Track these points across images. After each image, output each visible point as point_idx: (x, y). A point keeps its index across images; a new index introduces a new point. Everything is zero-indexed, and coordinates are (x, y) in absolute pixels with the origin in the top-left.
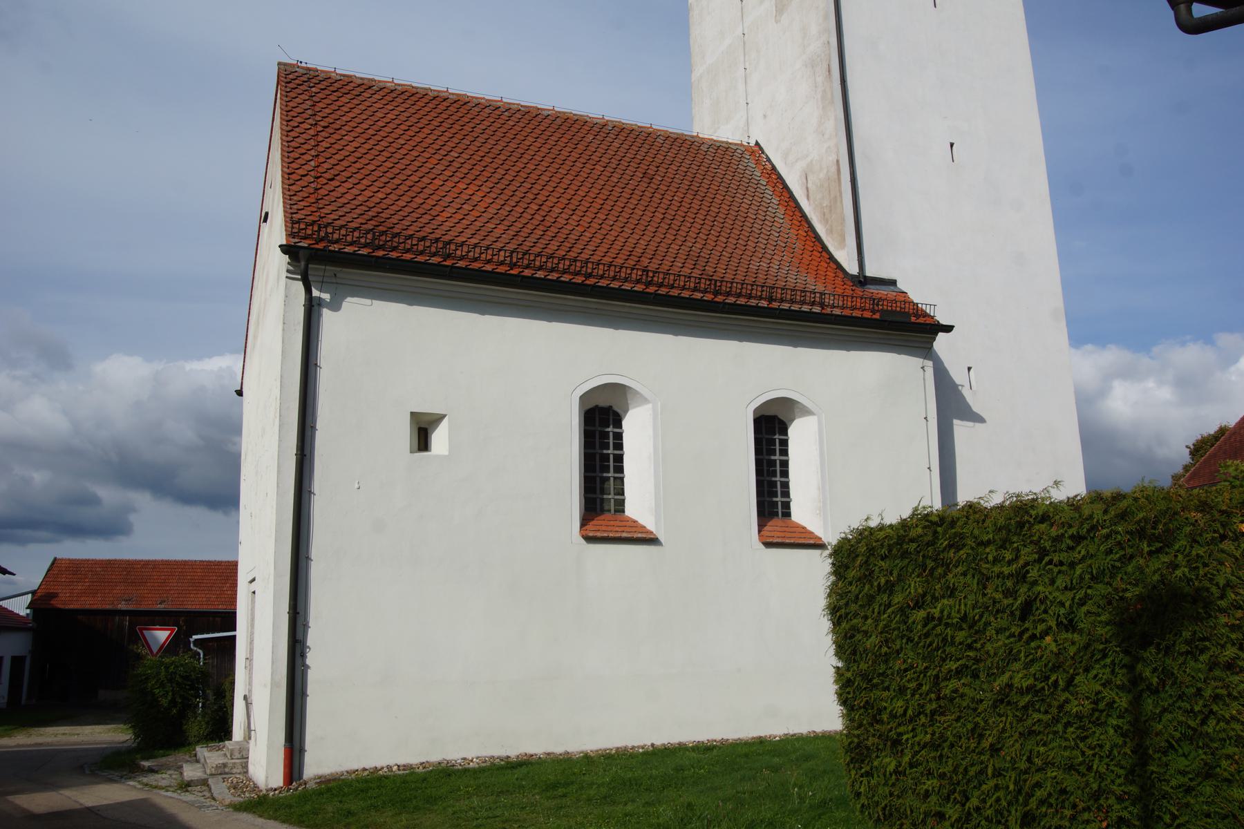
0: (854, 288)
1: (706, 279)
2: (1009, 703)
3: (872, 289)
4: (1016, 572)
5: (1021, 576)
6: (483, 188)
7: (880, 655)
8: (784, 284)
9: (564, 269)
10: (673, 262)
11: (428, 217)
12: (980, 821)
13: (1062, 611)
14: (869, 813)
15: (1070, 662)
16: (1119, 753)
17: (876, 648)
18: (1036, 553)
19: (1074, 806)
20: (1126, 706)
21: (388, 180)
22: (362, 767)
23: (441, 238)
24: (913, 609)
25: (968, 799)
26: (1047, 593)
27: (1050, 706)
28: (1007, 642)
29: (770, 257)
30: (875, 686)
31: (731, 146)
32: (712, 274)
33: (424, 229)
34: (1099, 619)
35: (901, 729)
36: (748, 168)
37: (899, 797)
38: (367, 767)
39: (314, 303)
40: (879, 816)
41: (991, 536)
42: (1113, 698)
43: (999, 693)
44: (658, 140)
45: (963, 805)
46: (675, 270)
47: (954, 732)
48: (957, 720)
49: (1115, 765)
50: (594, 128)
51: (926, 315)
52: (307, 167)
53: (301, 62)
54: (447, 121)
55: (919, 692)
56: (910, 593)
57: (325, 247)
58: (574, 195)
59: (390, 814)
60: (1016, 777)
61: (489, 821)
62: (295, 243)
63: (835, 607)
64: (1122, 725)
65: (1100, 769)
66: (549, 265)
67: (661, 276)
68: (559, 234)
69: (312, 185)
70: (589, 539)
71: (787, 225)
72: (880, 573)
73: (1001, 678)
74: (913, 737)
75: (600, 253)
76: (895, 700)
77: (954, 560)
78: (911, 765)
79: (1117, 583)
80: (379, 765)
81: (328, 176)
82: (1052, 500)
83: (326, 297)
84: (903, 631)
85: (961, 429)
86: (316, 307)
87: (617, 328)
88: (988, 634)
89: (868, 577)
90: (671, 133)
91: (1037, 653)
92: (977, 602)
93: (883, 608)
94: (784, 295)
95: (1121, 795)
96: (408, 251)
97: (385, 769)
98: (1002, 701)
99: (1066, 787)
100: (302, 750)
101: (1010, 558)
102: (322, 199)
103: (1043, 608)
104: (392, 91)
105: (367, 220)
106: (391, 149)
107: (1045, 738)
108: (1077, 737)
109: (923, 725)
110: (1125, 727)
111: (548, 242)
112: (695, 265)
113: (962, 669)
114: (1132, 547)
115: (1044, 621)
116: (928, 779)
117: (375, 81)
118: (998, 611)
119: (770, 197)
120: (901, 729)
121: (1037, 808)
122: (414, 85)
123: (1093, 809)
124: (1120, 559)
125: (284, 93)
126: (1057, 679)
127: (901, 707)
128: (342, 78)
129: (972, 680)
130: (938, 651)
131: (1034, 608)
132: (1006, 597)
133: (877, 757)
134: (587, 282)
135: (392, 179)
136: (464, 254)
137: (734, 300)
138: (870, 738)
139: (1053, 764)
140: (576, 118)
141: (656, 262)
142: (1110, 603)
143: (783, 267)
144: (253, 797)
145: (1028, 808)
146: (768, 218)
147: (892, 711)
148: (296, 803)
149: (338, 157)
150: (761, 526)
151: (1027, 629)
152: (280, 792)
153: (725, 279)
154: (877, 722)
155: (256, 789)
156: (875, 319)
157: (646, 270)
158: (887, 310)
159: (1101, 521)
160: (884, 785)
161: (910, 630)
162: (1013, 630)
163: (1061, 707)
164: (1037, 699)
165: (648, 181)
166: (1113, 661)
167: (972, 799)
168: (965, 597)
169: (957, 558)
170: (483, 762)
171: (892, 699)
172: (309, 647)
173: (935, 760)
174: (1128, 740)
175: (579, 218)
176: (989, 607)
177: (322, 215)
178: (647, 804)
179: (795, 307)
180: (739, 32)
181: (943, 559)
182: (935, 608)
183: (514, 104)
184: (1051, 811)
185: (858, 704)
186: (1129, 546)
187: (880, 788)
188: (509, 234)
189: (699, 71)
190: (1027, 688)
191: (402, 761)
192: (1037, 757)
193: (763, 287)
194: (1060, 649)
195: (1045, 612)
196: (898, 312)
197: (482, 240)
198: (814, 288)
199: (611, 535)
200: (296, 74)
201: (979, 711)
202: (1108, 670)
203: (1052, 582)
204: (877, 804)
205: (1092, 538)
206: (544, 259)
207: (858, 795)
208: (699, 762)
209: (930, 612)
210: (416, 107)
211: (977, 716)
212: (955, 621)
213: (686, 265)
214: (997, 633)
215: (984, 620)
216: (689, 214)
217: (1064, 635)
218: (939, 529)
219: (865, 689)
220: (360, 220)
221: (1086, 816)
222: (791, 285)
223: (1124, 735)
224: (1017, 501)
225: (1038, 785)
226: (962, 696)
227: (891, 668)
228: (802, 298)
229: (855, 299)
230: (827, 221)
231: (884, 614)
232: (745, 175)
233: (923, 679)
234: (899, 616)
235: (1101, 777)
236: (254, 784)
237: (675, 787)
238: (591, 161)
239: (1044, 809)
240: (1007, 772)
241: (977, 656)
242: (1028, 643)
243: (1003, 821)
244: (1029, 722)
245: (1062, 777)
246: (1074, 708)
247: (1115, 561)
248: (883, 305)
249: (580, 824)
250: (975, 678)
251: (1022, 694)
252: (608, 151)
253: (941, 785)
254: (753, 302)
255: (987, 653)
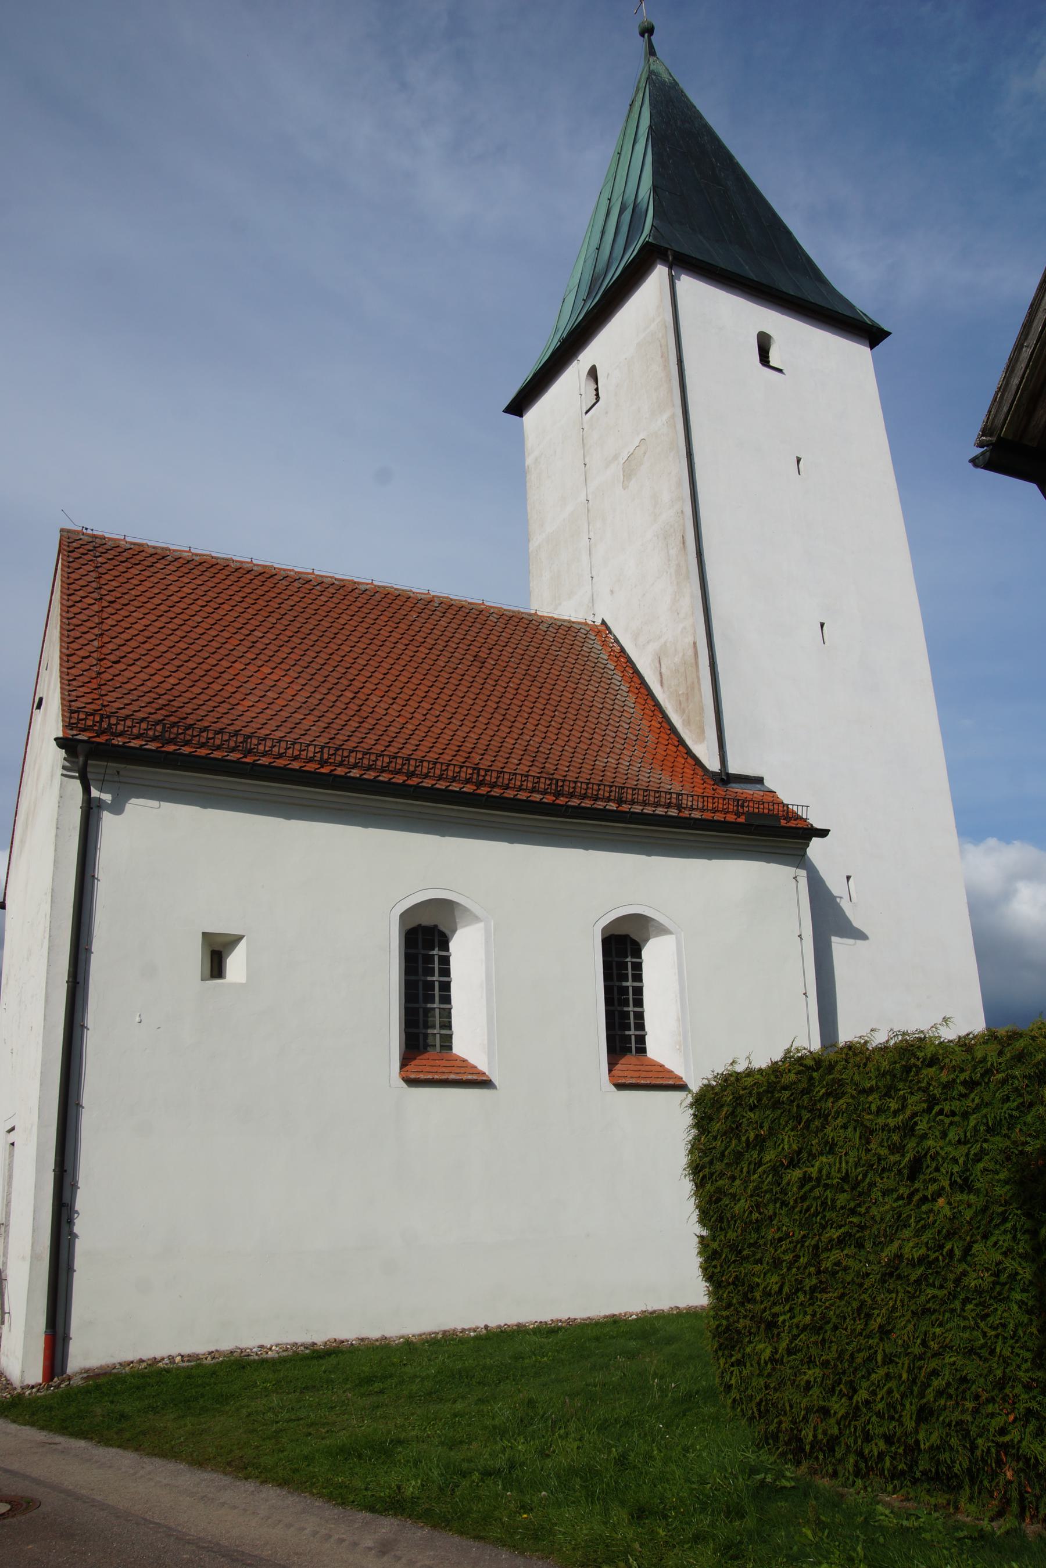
0: (715, 787)
1: (546, 778)
2: (899, 1277)
3: (736, 788)
4: (903, 1124)
5: (908, 1129)
6: (291, 673)
7: (751, 1221)
8: (636, 783)
9: (382, 767)
10: (508, 758)
11: (226, 706)
12: (870, 1418)
13: (956, 1169)
14: (742, 1410)
15: (966, 1228)
16: (1025, 1333)
17: (746, 1215)
18: (924, 1101)
19: (977, 1397)
20: (1030, 1278)
21: (181, 663)
22: (138, 1358)
23: (241, 730)
24: (787, 1167)
25: (855, 1391)
26: (938, 1148)
27: (945, 1279)
28: (895, 1205)
29: (619, 752)
30: (746, 1258)
31: (574, 625)
32: (553, 772)
33: (222, 720)
34: (997, 1177)
35: (776, 1309)
36: (593, 650)
37: (776, 1390)
38: (144, 1358)
39: (93, 805)
40: (753, 1413)
41: (874, 1082)
42: (1016, 1269)
43: (888, 1265)
44: (491, 618)
45: (851, 1398)
46: (510, 768)
47: (838, 1312)
48: (841, 1297)
49: (1021, 1348)
50: (418, 605)
51: (798, 818)
52: (89, 648)
53: (86, 529)
54: (251, 596)
55: (796, 1265)
56: (783, 1149)
57: (107, 740)
58: (394, 681)
59: (172, 1416)
60: (909, 1364)
61: (292, 1425)
62: (73, 735)
63: (697, 1166)
64: (1026, 1300)
65: (1004, 1352)
66: (366, 761)
67: (495, 774)
68: (377, 726)
69: (95, 669)
70: (411, 1082)
71: (638, 714)
72: (748, 1126)
73: (889, 1248)
74: (791, 1318)
75: (424, 748)
76: (769, 1275)
77: (833, 1111)
78: (790, 1352)
79: (1016, 1135)
80: (158, 1354)
81: (112, 658)
82: (942, 1040)
83: (107, 797)
84: (777, 1193)
85: (840, 947)
86: (95, 810)
87: (443, 835)
88: (873, 1196)
89: (734, 1131)
90: (505, 610)
91: (928, 1218)
92: (860, 1159)
93: (752, 1166)
94: (636, 796)
95: (1028, 1382)
96: (203, 745)
97: (166, 1361)
98: (891, 1274)
99: (967, 1374)
100: (66, 1338)
101: (896, 1107)
102: (105, 684)
103: (934, 1165)
104: (189, 562)
105: (157, 710)
106: (186, 628)
107: (941, 1317)
108: (978, 1315)
109: (801, 1304)
110: (1030, 1303)
111: (364, 736)
112: (533, 761)
113: (845, 1237)
114: (1030, 1094)
115: (935, 1180)
116: (809, 1368)
117: (170, 550)
118: (884, 1170)
119: (619, 684)
120: (776, 1309)
121: (935, 1400)
122: (214, 554)
123: (998, 1400)
124: (1017, 1108)
125: (67, 564)
126: (952, 1248)
127: (776, 1283)
128: (132, 546)
129: (856, 1250)
130: (816, 1217)
131: (924, 1166)
132: (893, 1154)
133: (750, 1342)
134: (409, 782)
135: (186, 662)
136: (267, 749)
137: (579, 802)
138: (741, 1320)
139: (951, 1348)
140: (397, 593)
141: (489, 758)
142: (1008, 1159)
143: (634, 763)
144: (5, 1397)
145: (925, 1400)
146: (616, 707)
147: (765, 1288)
148: (58, 1404)
149: (125, 636)
150: (612, 1065)
151: (917, 1190)
152: (38, 1391)
153: (568, 778)
154: (749, 1301)
155: (9, 1386)
156: (740, 824)
157: (476, 769)
158: (753, 813)
159: (995, 1064)
160: (759, 1375)
161: (784, 1192)
162: (901, 1192)
163: (958, 1281)
164: (930, 1271)
165: (480, 665)
166: (1014, 1225)
167: (861, 1392)
168: (846, 1154)
169: (835, 1108)
170: (284, 1351)
171: (765, 1274)
172: (77, 1212)
173: (817, 1345)
174: (1034, 1317)
175: (400, 708)
176: (873, 1165)
177: (105, 703)
178: (481, 1401)
179: (648, 810)
180: (583, 498)
181: (820, 1110)
182: (813, 1166)
183: (327, 577)
184: (950, 1403)
185: (727, 1280)
186: (1028, 1092)
187: (754, 1380)
188: (319, 726)
189: (537, 540)
190: (919, 1259)
191: (187, 1350)
192: (933, 1340)
193: (611, 787)
194: (954, 1213)
195: (937, 1170)
196: (766, 815)
197: (289, 733)
198: (670, 787)
199: (436, 1077)
200: (81, 542)
201: (865, 1286)
202: (1009, 1236)
203: (944, 1135)
204: (751, 1398)
205: (987, 1084)
206: (360, 756)
207: (728, 1388)
208: (541, 1348)
209: (806, 1172)
210: (215, 580)
211: (863, 1293)
212: (835, 1181)
213: (522, 761)
214: (884, 1195)
215: (868, 1180)
216: (526, 703)
217: (959, 1197)
218: (815, 1074)
219: (734, 1262)
220: (148, 710)
221: (990, 1408)
222: (643, 785)
223: (1029, 1312)
224: (901, 1041)
225: (935, 1373)
226: (846, 1269)
227: (763, 1237)
228: (656, 800)
229: (716, 800)
230: (683, 711)
231: (754, 1174)
232: (590, 658)
233: (800, 1250)
234: (771, 1176)
235: (1005, 1362)
236: (7, 1380)
237: (514, 1380)
238: (414, 643)
239: (942, 1402)
240: (899, 1358)
241: (861, 1222)
242: (918, 1206)
243: (897, 1416)
244: (923, 1298)
245: (962, 1363)
246: (972, 1281)
247: (1012, 1110)
248: (748, 806)
249: (401, 1427)
250: (859, 1248)
251: (914, 1266)
252: (434, 631)
253: (824, 1375)
254: (600, 805)
255: (873, 1218)
